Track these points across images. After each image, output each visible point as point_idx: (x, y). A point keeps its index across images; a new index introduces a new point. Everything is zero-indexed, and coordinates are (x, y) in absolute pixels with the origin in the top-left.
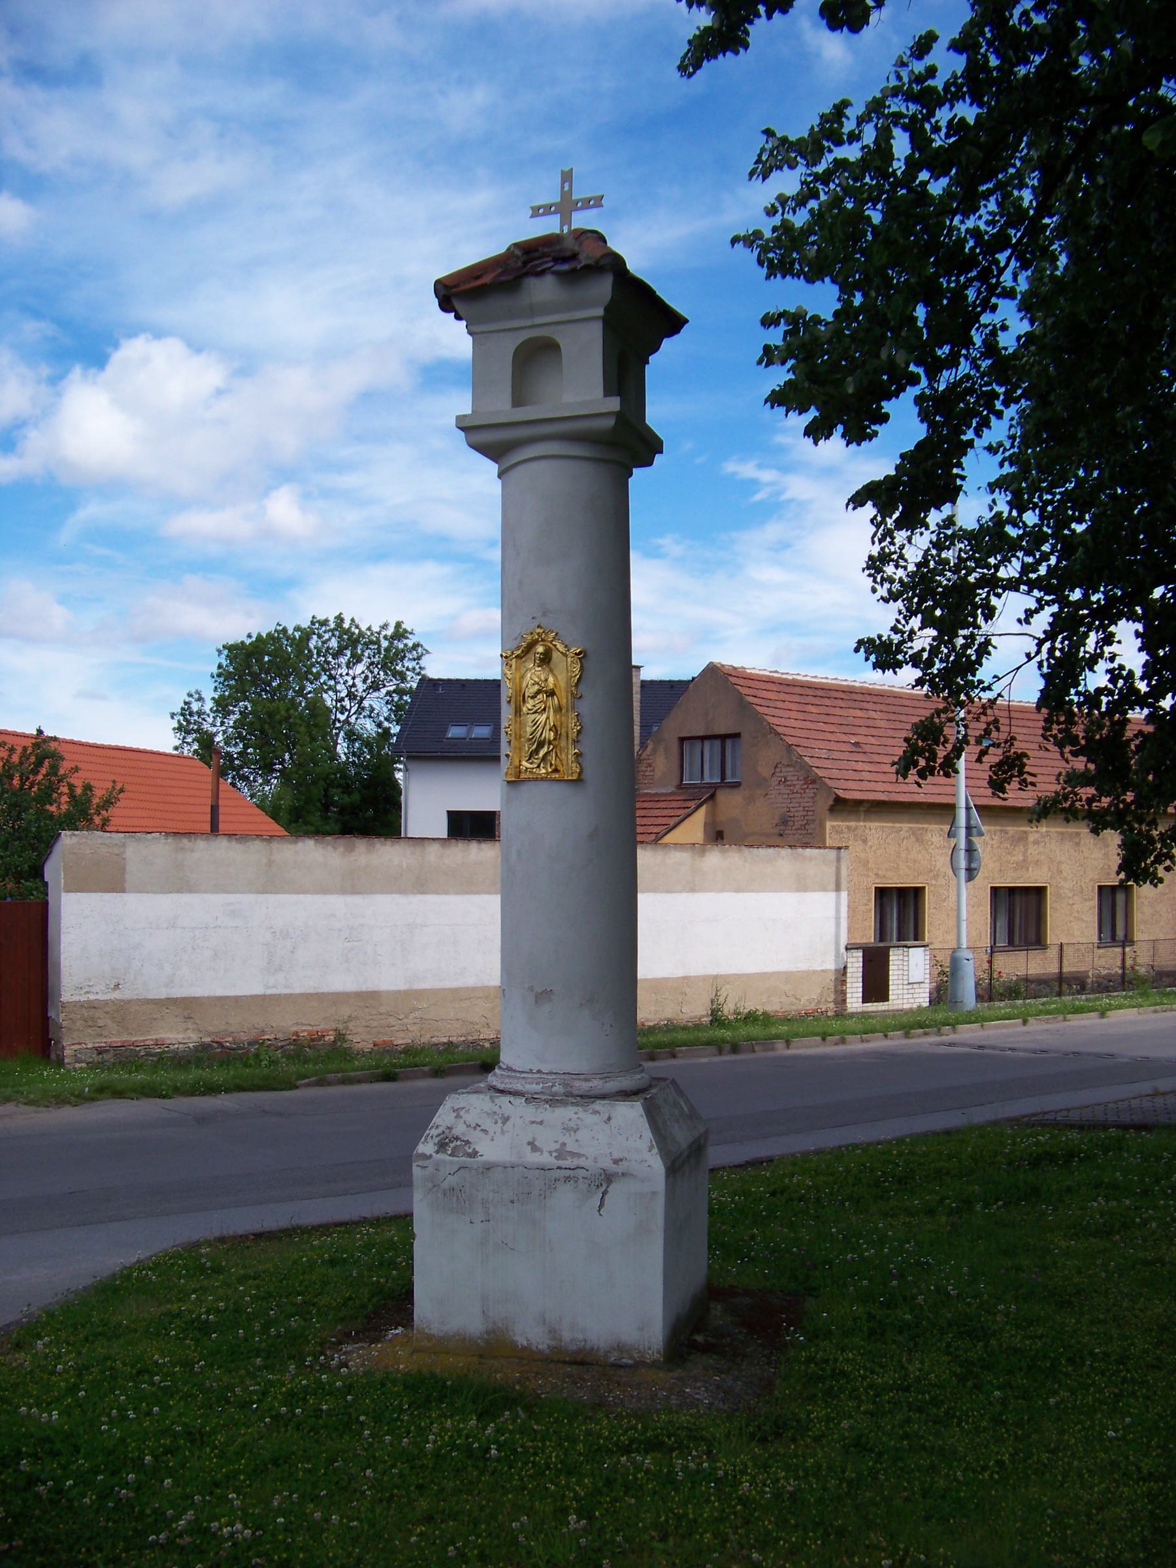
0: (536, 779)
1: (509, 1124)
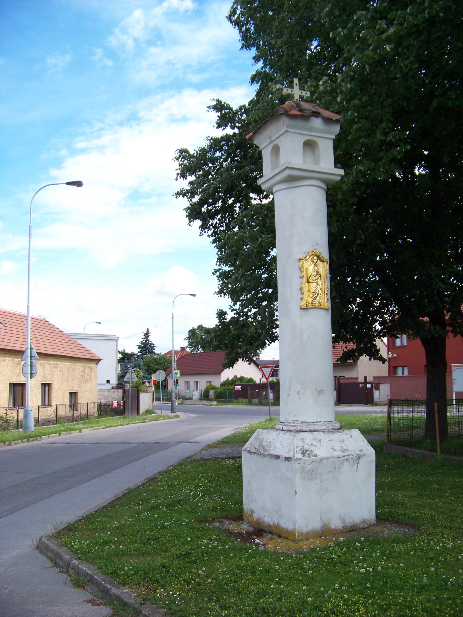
0: (316, 308)
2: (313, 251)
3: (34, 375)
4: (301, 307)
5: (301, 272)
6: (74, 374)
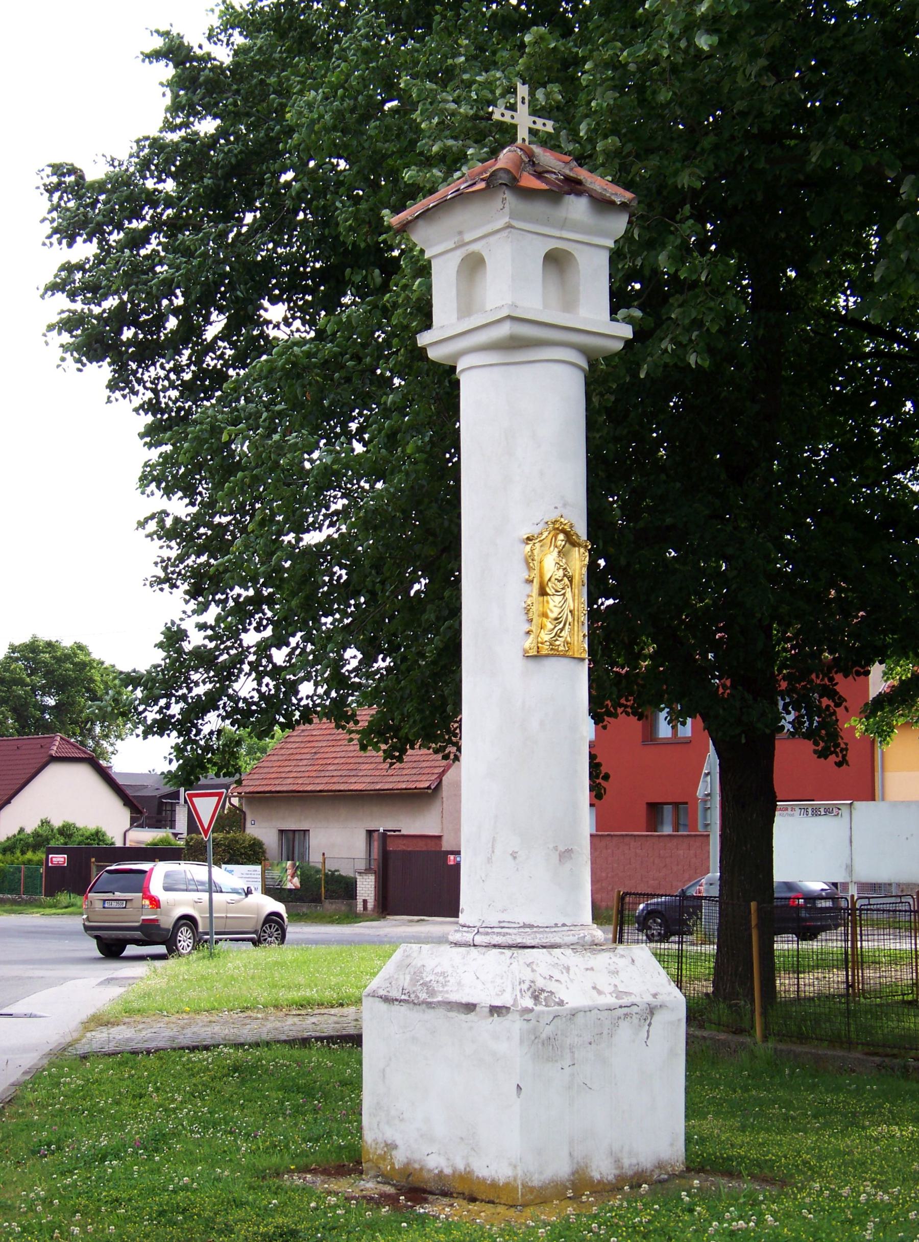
0: (559, 656)
1: (571, 972)
2: (556, 521)
4: (525, 651)
5: (530, 568)
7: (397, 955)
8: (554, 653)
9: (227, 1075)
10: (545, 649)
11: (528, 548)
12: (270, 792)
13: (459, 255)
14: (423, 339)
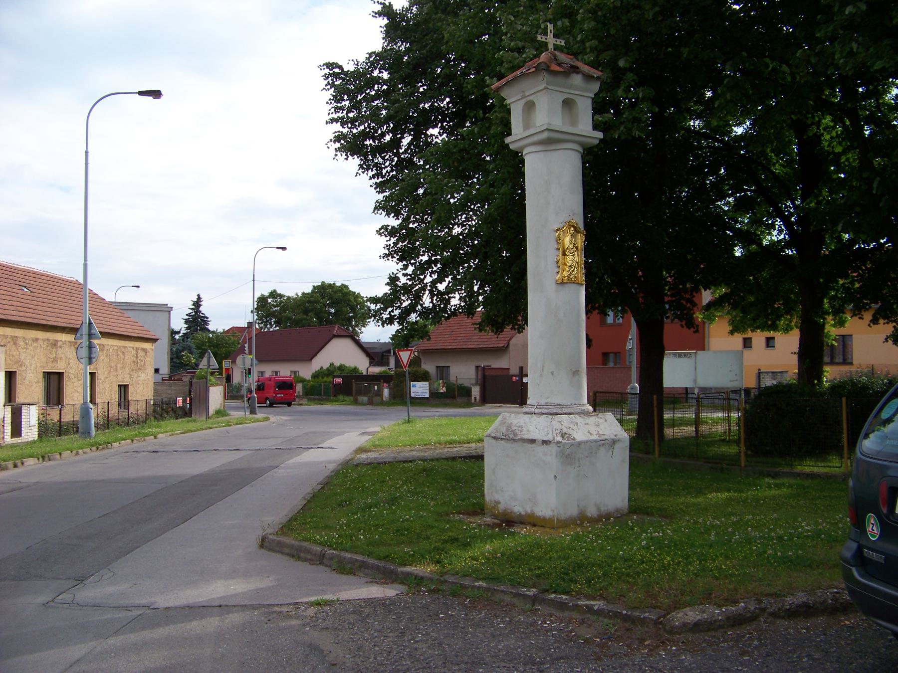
0: (572, 283)
3: (94, 360)
4: (557, 281)
5: (558, 243)
6: (124, 359)
7: (500, 418)
8: (570, 282)
9: (421, 473)
10: (566, 280)
11: (557, 234)
12: (432, 349)
13: (523, 102)
14: (508, 140)
